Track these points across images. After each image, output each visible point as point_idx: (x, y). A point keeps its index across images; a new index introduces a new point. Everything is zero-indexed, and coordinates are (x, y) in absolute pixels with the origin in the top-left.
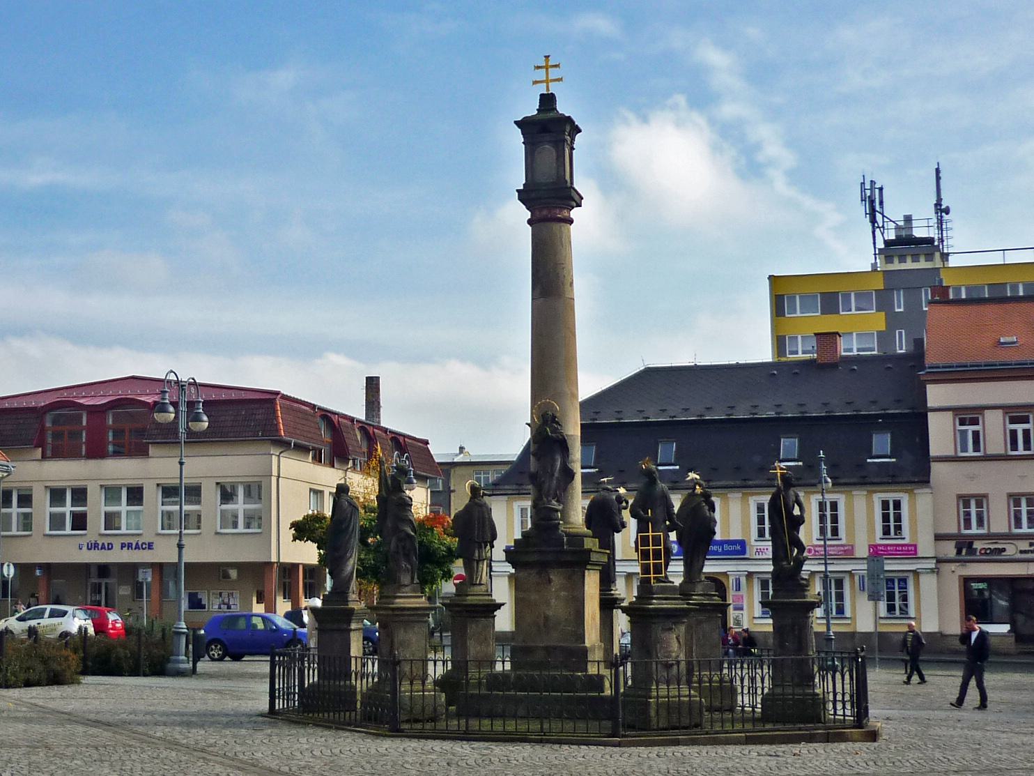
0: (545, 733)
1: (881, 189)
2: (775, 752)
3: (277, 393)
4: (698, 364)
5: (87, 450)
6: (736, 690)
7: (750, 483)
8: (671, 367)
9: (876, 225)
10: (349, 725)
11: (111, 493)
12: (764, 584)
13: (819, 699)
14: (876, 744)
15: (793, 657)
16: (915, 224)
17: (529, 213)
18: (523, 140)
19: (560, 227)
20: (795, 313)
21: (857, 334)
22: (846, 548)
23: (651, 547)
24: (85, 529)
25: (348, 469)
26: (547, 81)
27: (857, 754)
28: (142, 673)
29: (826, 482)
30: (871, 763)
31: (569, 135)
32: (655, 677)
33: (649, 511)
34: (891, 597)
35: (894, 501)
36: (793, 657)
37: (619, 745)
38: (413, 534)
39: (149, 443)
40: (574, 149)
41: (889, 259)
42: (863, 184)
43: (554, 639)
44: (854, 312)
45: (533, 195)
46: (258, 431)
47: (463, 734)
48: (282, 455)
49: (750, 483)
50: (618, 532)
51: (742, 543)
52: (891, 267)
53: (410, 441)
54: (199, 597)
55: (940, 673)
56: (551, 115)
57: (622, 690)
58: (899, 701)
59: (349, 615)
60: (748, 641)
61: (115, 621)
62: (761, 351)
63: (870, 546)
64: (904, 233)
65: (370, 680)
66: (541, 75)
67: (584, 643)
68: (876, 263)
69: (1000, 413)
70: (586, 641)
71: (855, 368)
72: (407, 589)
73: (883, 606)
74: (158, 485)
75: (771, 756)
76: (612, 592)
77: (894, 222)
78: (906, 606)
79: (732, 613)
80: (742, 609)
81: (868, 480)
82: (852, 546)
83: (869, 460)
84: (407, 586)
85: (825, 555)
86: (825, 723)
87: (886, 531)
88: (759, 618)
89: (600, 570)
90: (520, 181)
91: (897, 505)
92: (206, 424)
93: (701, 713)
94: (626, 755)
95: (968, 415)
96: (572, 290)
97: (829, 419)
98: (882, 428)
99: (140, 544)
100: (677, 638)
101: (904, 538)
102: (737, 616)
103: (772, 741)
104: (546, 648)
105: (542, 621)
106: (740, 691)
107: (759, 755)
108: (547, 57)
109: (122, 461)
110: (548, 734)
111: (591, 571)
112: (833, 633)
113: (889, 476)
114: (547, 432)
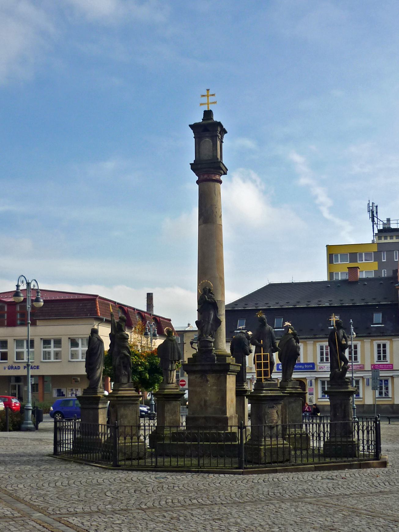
0: (200, 467)
1: (377, 207)
2: (331, 477)
3: (97, 296)
4: (294, 282)
5: (7, 322)
6: (309, 438)
7: (317, 336)
8: (281, 283)
9: (374, 223)
10: (92, 462)
11: (19, 343)
12: (323, 383)
13: (355, 444)
14: (386, 469)
15: (342, 422)
16: (391, 222)
17: (197, 178)
18: (194, 136)
19: (215, 185)
20: (338, 262)
21: (365, 272)
22: (361, 366)
23: (262, 361)
24: (7, 360)
25: (132, 332)
27: (378, 476)
28: (8, 430)
29: (353, 334)
30: (387, 483)
31: (220, 133)
32: (264, 434)
33: (262, 341)
34: (381, 388)
35: (383, 344)
36: (342, 422)
37: (242, 473)
38: (128, 355)
39: (37, 319)
40: (223, 142)
41: (380, 238)
42: (369, 204)
43: (210, 412)
44: (364, 261)
45: (199, 166)
46: (88, 314)
47: (154, 468)
48: (99, 325)
49: (317, 336)
50: (248, 355)
51: (313, 364)
52: (380, 241)
53: (162, 319)
54: (62, 391)
55: (81, 324)
56: (210, 121)
57: (244, 442)
58: (390, 440)
59: (97, 400)
60: (316, 410)
61: (16, 403)
62: (322, 276)
63: (372, 365)
64: (386, 226)
65: (106, 436)
66: (204, 100)
67: (226, 415)
68: (374, 240)
70: (227, 414)
71: (366, 283)
72: (125, 386)
73: (377, 392)
74: (41, 339)
75: (329, 479)
76: (244, 387)
77: (382, 221)
78: (388, 392)
79: (308, 396)
80: (312, 394)
81: (372, 335)
82: (364, 365)
83: (372, 326)
84: (126, 384)
85: (352, 369)
86: (358, 457)
87: (379, 358)
88: (320, 398)
89: (236, 375)
90: (192, 159)
91: (384, 346)
92: (42, 304)
93: (290, 452)
94: (245, 481)
96: (221, 220)
97: (354, 307)
98: (378, 311)
99: (33, 366)
100: (277, 412)
101: (387, 361)
102: (310, 398)
103: (329, 469)
104: (205, 418)
105: (203, 403)
106: (311, 438)
107: (322, 479)
108: (208, 90)
109: (24, 327)
110: (202, 467)
111: (230, 375)
112: (356, 405)
113: (381, 333)
114: (206, 298)
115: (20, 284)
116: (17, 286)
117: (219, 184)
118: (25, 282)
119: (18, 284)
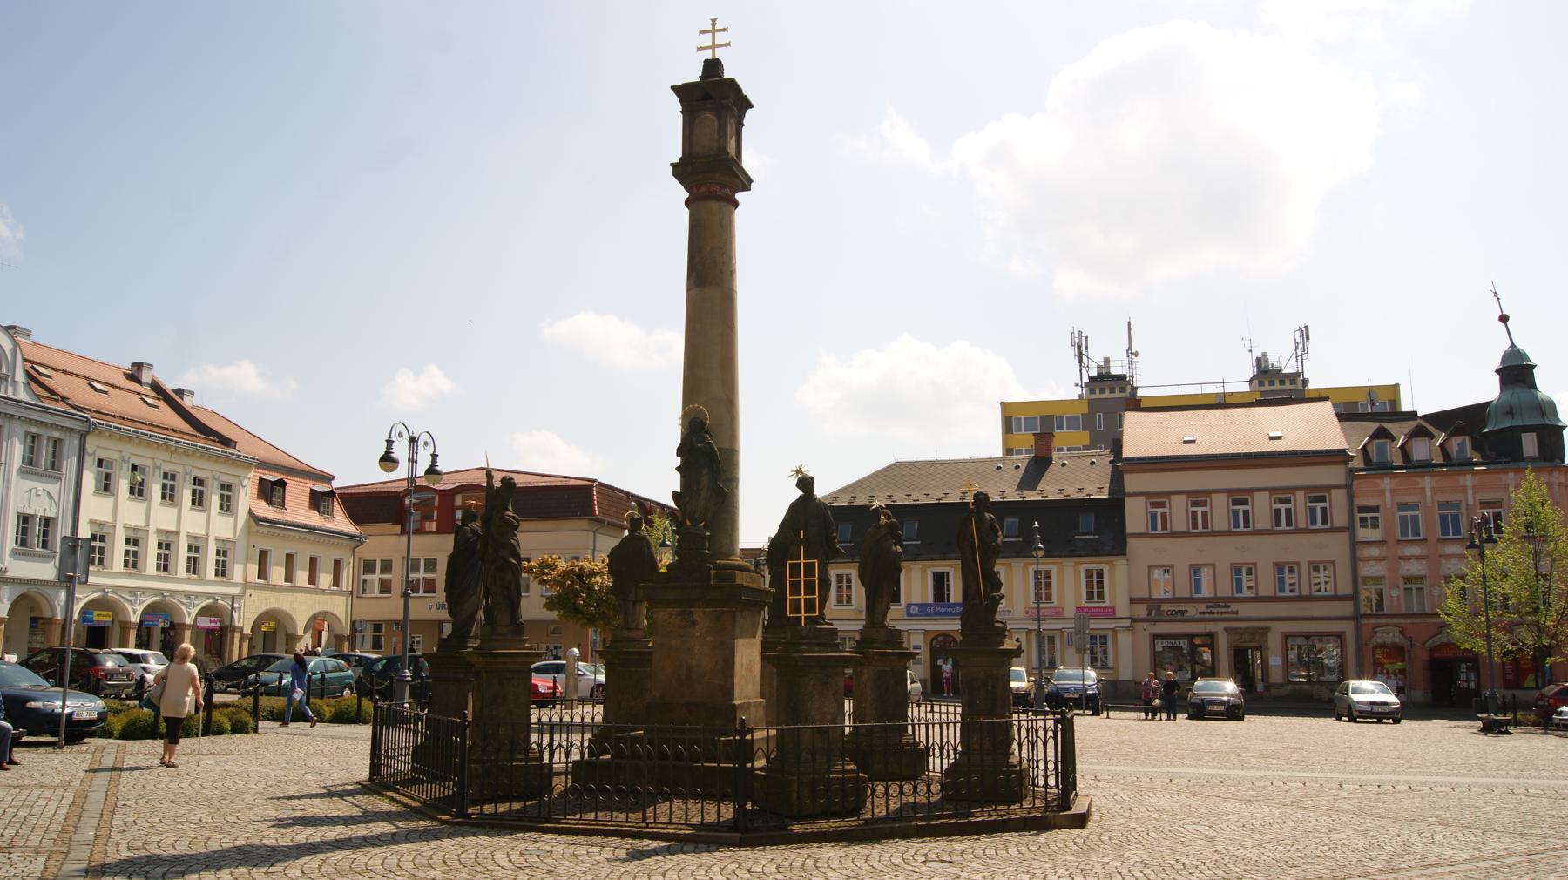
0: (648, 823)
1: (1086, 338)
3: (594, 481)
14: (1084, 832)
16: (1111, 364)
26: (713, 47)
33: (802, 532)
42: (1073, 333)
52: (1093, 396)
66: (706, 40)
68: (1082, 394)
69: (1183, 497)
75: (942, 861)
78: (1106, 658)
83: (1077, 537)
95: (1158, 499)
115: (393, 438)
116: (387, 441)
117: (732, 207)
118: (406, 436)
119: (390, 437)
